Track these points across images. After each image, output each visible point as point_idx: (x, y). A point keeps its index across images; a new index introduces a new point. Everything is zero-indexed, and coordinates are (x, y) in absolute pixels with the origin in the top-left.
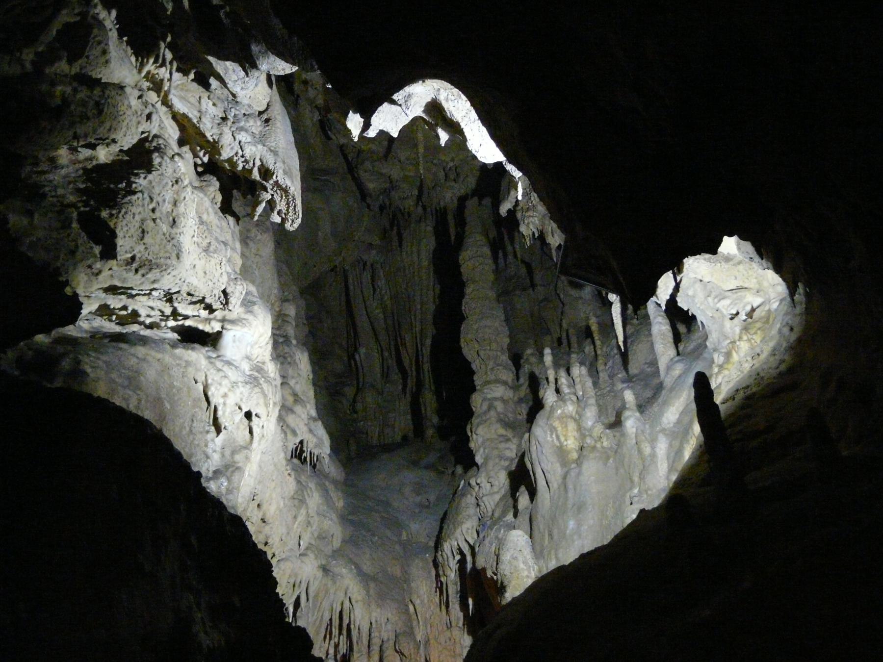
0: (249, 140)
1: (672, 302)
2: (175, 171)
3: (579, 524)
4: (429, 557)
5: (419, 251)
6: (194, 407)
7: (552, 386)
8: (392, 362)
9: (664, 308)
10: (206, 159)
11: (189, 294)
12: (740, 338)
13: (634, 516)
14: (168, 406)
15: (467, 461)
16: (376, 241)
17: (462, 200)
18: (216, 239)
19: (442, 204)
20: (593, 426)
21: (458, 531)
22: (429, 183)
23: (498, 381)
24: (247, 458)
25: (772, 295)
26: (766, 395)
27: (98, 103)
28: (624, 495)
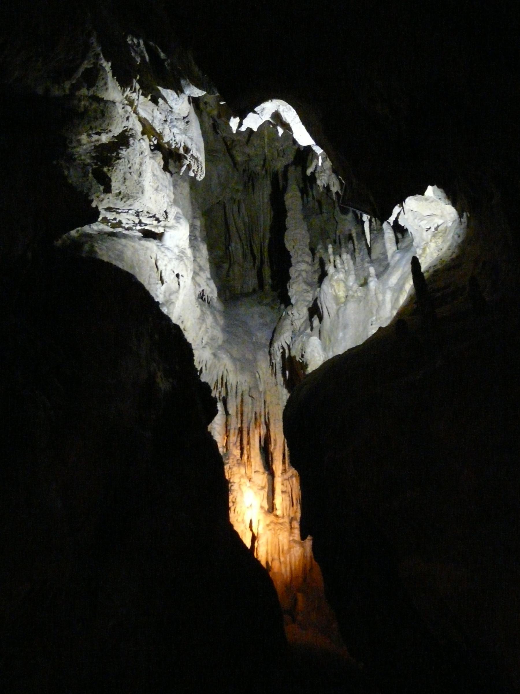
0: (178, 132)
1: (396, 221)
2: (141, 148)
3: (344, 335)
4: (267, 350)
5: (263, 194)
6: (151, 270)
7: (332, 264)
8: (248, 251)
9: (392, 224)
10: (156, 142)
11: (148, 213)
12: (431, 241)
13: (374, 331)
14: (137, 270)
15: (286, 301)
16: (240, 188)
17: (286, 167)
18: (162, 184)
19: (276, 169)
20: (353, 285)
21: (282, 338)
22: (269, 158)
23: (304, 261)
24: (177, 298)
25: (449, 219)
26: (447, 268)
27: (102, 110)
28: (368, 320)
